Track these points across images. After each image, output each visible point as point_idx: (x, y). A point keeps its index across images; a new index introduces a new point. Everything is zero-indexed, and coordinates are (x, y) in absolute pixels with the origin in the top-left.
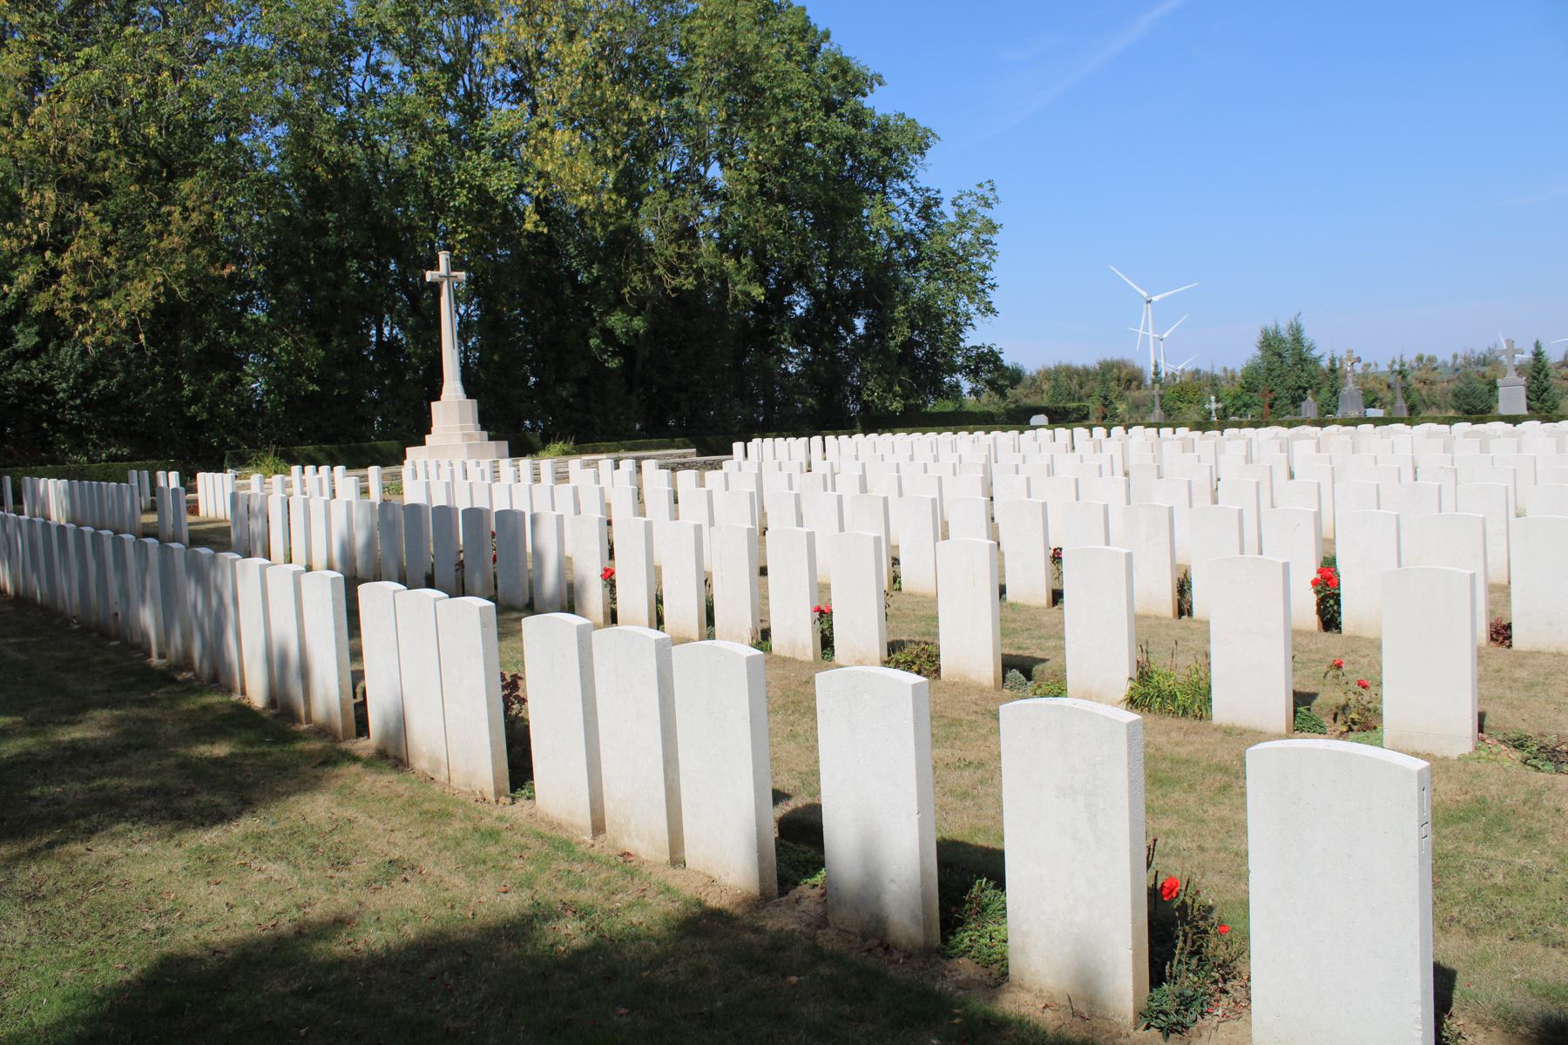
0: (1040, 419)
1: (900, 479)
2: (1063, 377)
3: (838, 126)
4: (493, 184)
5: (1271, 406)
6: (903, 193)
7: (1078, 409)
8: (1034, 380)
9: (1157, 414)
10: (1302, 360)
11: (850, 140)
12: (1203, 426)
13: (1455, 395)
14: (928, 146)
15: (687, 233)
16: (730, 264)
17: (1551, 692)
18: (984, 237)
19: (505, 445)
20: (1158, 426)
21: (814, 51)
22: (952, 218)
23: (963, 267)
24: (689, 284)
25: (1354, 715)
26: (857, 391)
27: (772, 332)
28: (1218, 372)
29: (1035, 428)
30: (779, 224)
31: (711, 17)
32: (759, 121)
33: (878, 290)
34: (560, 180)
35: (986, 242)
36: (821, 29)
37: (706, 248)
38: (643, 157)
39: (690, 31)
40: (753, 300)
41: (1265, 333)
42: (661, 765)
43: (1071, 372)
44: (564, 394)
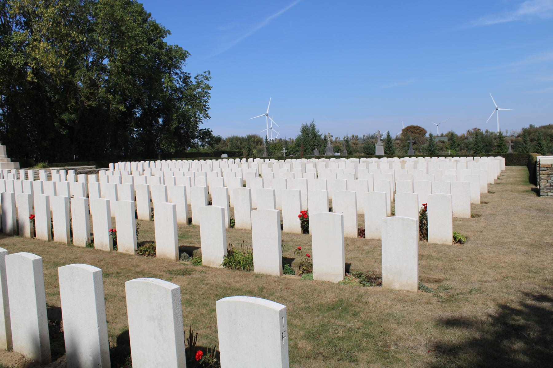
0: (225, 155)
1: (175, 178)
2: (235, 140)
3: (152, 47)
4: (14, 61)
5: (305, 151)
6: (177, 74)
7: (239, 152)
8: (224, 141)
9: (265, 154)
10: (316, 136)
11: (157, 54)
12: (279, 158)
13: (364, 148)
14: (186, 57)
15: (93, 84)
16: (111, 97)
17: (375, 254)
18: (206, 90)
19: (18, 164)
20: (264, 158)
21: (145, 21)
22: (194, 83)
23: (198, 101)
24: (94, 104)
25: (304, 268)
26: (158, 144)
27: (128, 123)
28: (288, 139)
29: (222, 159)
30: (130, 83)
31: (105, 4)
32: (122, 44)
33: (168, 107)
34: (42, 62)
35: (206, 93)
36: (148, 12)
37: (102, 91)
38: (78, 55)
39: (96, 9)
40: (119, 111)
41: (303, 126)
42: (3, 306)
43: (237, 139)
44: (45, 145)
